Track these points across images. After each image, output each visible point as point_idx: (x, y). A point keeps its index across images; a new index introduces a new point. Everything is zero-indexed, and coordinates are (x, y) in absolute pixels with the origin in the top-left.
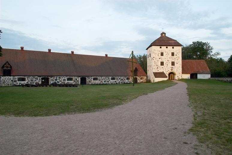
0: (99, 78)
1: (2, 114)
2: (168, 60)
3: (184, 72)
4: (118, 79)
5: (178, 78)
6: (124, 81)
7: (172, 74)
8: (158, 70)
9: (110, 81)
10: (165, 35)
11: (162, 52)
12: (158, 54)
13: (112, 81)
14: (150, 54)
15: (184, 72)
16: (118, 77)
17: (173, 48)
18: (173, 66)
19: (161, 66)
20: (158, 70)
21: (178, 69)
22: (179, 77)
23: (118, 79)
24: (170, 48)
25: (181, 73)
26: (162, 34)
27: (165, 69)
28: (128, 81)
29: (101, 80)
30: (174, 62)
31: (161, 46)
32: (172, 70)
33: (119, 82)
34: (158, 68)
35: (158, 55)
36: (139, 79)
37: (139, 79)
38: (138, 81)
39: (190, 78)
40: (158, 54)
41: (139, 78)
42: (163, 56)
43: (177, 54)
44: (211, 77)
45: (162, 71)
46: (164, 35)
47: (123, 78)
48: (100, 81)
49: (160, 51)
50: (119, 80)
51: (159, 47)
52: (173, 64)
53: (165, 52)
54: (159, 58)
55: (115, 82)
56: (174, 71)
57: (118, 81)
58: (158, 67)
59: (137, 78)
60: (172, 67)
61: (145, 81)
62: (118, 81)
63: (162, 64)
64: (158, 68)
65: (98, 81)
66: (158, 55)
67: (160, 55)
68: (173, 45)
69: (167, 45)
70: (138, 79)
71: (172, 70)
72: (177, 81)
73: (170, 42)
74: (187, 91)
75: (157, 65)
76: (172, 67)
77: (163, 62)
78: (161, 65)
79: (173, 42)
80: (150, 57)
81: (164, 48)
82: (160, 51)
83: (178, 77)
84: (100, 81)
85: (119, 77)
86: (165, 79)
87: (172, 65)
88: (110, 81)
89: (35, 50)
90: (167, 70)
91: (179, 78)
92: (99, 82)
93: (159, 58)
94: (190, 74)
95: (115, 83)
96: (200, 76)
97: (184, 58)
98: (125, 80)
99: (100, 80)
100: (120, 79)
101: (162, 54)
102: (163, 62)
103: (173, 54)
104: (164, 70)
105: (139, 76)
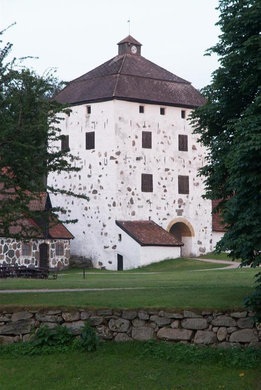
1: (1, 277)
2: (167, 170)
11: (147, 130)
12: (133, 138)
20: (133, 214)
22: (203, 246)
25: (210, 229)
26: (121, 45)
32: (180, 212)
34: (132, 201)
42: (180, 136)
45: (146, 219)
46: (134, 49)
51: (137, 106)
53: (159, 132)
54: (138, 159)
58: (135, 198)
64: (132, 201)
67: (139, 142)
71: (180, 212)
73: (173, 86)
76: (180, 201)
77: (151, 176)
78: (187, 178)
79: (180, 87)
81: (152, 111)
89: (158, 65)
90: (163, 214)
91: (204, 250)
93: (138, 159)
102: (151, 176)
104: (155, 211)
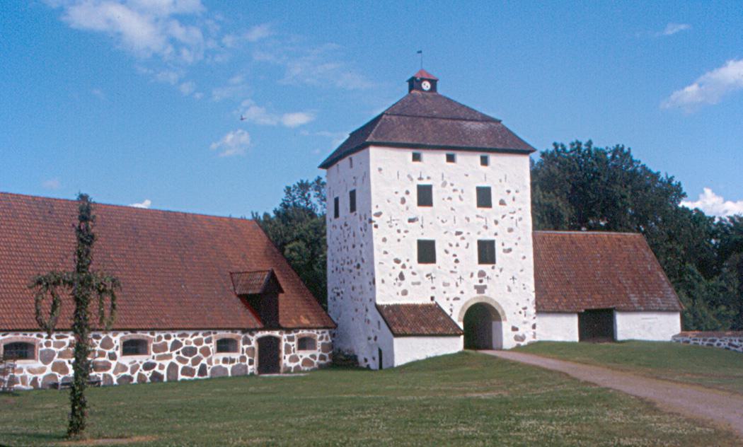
0: (153, 338)
2: (458, 233)
3: (546, 304)
4: (164, 347)
5: (517, 338)
6: (204, 361)
7: (481, 321)
8: (405, 293)
9: (114, 363)
10: (433, 88)
11: (425, 182)
13: (127, 361)
14: (353, 194)
15: (546, 304)
16: (168, 337)
17: (484, 162)
18: (486, 268)
19: (422, 266)
21: (513, 288)
22: (519, 333)
23: (164, 347)
24: (468, 162)
25: (532, 310)
27: (445, 285)
28: (225, 361)
29: (56, 359)
30: (492, 243)
31: (417, 147)
32: (481, 289)
33: (173, 367)
34: (402, 277)
35: (403, 201)
36: (288, 349)
37: (288, 349)
38: (286, 361)
39: (576, 339)
40: (402, 194)
41: (291, 339)
43: (508, 200)
44: (685, 327)
47: (198, 342)
48: (49, 367)
49: (415, 177)
50: (170, 356)
52: (486, 252)
55: (148, 366)
56: (495, 294)
57: (166, 363)
58: (407, 273)
59: (278, 340)
60: (482, 274)
61: (322, 357)
62: (166, 363)
63: (427, 252)
64: (402, 277)
65: (38, 364)
66: (403, 201)
68: (486, 146)
69: (452, 148)
70: (283, 344)
71: (481, 289)
72: (507, 353)
74: (275, 211)
75: (397, 261)
76: (482, 274)
80: (353, 208)
81: (434, 162)
82: (415, 177)
83: (514, 329)
84: (49, 367)
85: (175, 336)
86: (456, 345)
87: (491, 244)
88: (114, 363)
91: (523, 339)
92: (42, 370)
94: (581, 316)
95: (148, 374)
96: (629, 327)
97: (545, 217)
98: (206, 352)
99: (47, 358)
100: (176, 345)
101: (425, 196)
103: (484, 197)
105: (288, 330)
